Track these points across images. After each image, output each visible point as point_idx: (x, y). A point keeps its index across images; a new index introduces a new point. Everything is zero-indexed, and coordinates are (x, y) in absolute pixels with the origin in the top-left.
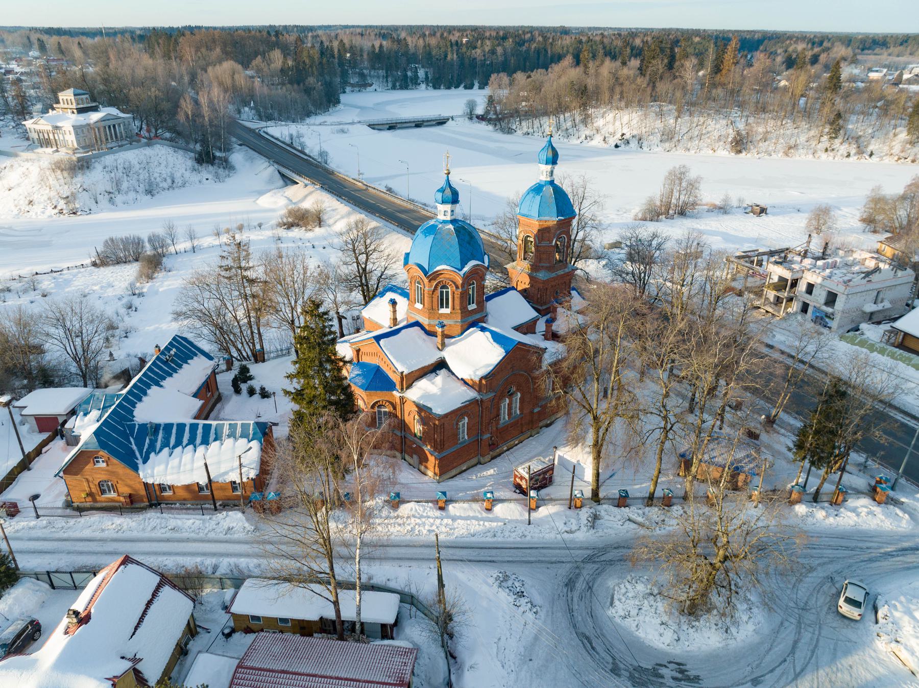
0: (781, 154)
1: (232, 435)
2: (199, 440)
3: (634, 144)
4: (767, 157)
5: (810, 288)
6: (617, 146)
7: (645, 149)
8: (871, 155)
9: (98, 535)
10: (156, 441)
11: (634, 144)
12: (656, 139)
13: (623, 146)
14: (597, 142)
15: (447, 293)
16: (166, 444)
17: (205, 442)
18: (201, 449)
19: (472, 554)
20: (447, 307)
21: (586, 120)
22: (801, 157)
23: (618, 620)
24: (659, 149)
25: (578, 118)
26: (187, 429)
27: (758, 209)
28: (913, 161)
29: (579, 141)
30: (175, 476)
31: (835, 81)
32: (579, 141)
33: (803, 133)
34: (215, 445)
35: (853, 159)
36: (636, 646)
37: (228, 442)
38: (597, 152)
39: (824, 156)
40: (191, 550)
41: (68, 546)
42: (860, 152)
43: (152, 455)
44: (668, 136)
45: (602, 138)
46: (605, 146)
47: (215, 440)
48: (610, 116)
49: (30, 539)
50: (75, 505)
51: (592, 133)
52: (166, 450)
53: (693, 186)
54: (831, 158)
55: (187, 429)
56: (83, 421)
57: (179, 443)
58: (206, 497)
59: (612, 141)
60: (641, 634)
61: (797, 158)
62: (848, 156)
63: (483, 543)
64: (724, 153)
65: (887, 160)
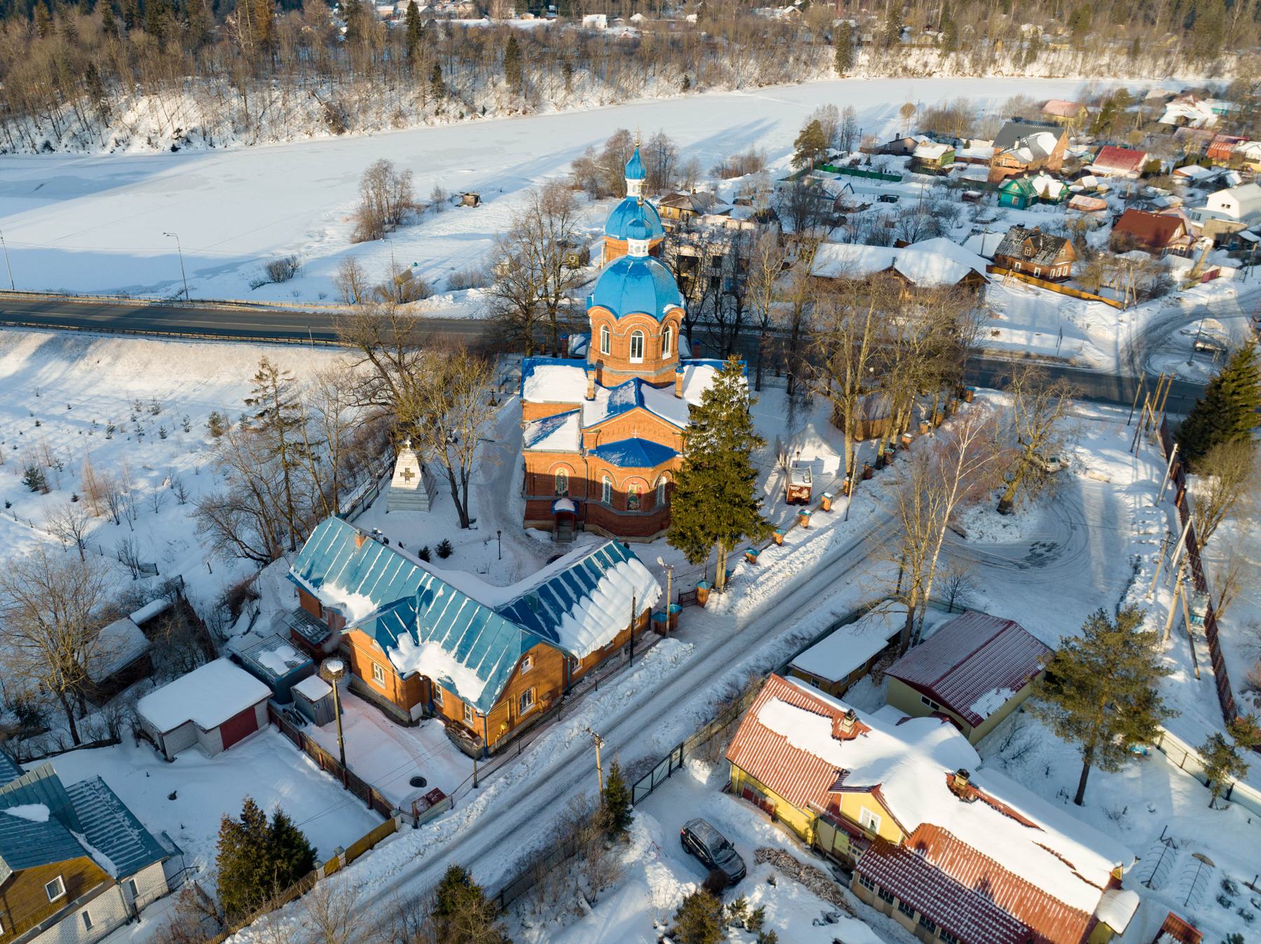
0: (390, 127)
1: (607, 565)
2: (584, 588)
3: (198, 143)
4: (376, 132)
5: (717, 261)
6: (174, 149)
7: (218, 147)
8: (484, 111)
9: (566, 753)
10: (547, 612)
11: (198, 143)
12: (227, 128)
13: (183, 147)
14: (138, 147)
15: (640, 340)
16: (559, 611)
17: (592, 586)
18: (594, 594)
19: (841, 566)
20: (640, 355)
21: (105, 114)
22: (414, 126)
23: (979, 542)
24: (238, 144)
25: (90, 115)
26: (562, 581)
27: (470, 199)
28: (524, 113)
29: (107, 151)
30: (603, 635)
31: (415, 26)
32: (107, 151)
33: (407, 98)
34: (601, 583)
35: (467, 119)
36: (1007, 548)
37: (610, 573)
38: (157, 164)
39: (437, 120)
40: (671, 699)
41: (560, 780)
42: (473, 110)
43: (557, 628)
44: (245, 123)
45: (146, 142)
46: (155, 151)
47: (598, 579)
48: (143, 104)
49: (512, 805)
50: (491, 750)
51: (123, 135)
52: (565, 616)
53: (402, 183)
54: (445, 122)
55: (562, 581)
56: (401, 654)
57: (570, 603)
58: (629, 646)
59: (165, 143)
60: (1000, 541)
61: (410, 128)
62: (462, 117)
63: (840, 549)
64: (324, 135)
65: (500, 116)
